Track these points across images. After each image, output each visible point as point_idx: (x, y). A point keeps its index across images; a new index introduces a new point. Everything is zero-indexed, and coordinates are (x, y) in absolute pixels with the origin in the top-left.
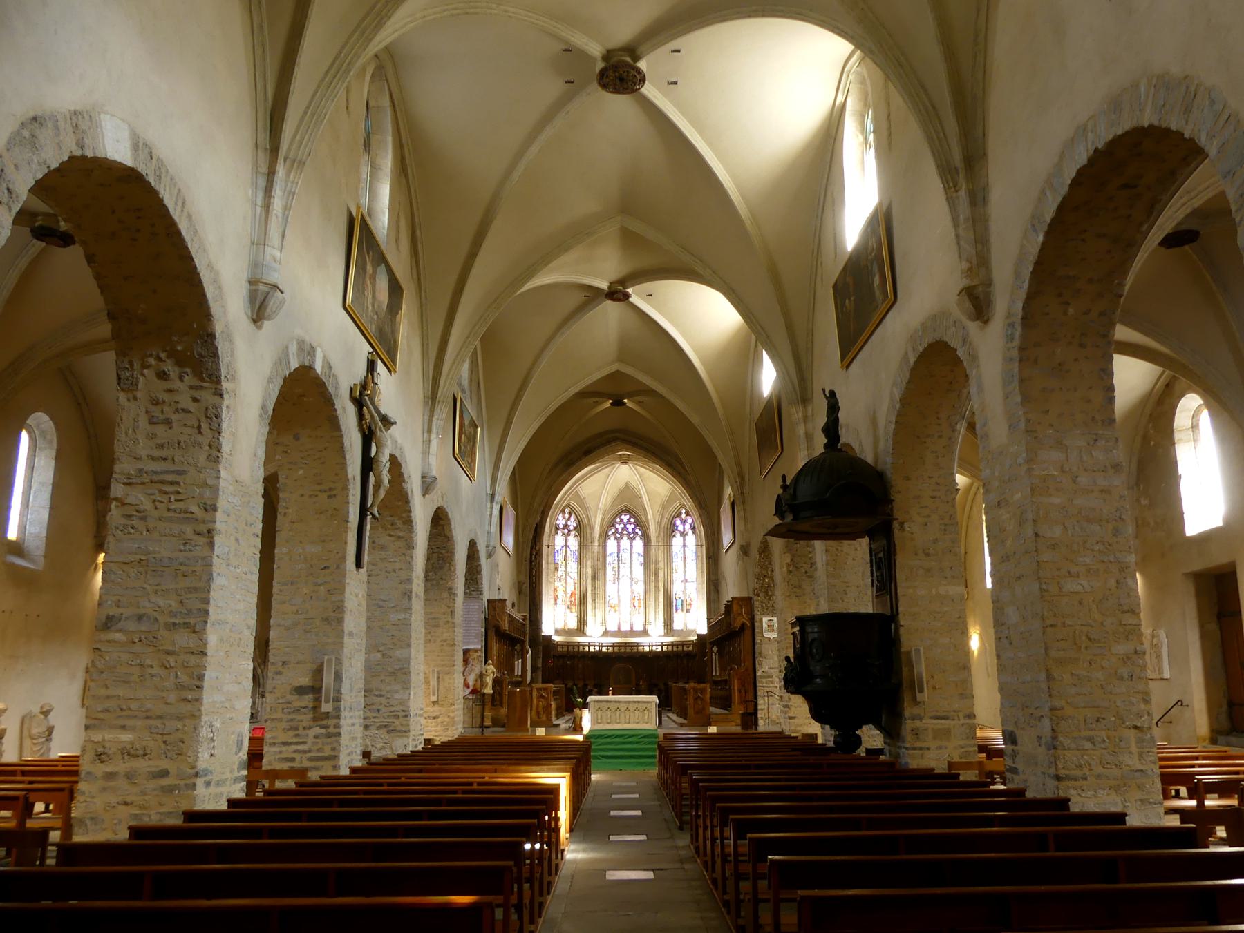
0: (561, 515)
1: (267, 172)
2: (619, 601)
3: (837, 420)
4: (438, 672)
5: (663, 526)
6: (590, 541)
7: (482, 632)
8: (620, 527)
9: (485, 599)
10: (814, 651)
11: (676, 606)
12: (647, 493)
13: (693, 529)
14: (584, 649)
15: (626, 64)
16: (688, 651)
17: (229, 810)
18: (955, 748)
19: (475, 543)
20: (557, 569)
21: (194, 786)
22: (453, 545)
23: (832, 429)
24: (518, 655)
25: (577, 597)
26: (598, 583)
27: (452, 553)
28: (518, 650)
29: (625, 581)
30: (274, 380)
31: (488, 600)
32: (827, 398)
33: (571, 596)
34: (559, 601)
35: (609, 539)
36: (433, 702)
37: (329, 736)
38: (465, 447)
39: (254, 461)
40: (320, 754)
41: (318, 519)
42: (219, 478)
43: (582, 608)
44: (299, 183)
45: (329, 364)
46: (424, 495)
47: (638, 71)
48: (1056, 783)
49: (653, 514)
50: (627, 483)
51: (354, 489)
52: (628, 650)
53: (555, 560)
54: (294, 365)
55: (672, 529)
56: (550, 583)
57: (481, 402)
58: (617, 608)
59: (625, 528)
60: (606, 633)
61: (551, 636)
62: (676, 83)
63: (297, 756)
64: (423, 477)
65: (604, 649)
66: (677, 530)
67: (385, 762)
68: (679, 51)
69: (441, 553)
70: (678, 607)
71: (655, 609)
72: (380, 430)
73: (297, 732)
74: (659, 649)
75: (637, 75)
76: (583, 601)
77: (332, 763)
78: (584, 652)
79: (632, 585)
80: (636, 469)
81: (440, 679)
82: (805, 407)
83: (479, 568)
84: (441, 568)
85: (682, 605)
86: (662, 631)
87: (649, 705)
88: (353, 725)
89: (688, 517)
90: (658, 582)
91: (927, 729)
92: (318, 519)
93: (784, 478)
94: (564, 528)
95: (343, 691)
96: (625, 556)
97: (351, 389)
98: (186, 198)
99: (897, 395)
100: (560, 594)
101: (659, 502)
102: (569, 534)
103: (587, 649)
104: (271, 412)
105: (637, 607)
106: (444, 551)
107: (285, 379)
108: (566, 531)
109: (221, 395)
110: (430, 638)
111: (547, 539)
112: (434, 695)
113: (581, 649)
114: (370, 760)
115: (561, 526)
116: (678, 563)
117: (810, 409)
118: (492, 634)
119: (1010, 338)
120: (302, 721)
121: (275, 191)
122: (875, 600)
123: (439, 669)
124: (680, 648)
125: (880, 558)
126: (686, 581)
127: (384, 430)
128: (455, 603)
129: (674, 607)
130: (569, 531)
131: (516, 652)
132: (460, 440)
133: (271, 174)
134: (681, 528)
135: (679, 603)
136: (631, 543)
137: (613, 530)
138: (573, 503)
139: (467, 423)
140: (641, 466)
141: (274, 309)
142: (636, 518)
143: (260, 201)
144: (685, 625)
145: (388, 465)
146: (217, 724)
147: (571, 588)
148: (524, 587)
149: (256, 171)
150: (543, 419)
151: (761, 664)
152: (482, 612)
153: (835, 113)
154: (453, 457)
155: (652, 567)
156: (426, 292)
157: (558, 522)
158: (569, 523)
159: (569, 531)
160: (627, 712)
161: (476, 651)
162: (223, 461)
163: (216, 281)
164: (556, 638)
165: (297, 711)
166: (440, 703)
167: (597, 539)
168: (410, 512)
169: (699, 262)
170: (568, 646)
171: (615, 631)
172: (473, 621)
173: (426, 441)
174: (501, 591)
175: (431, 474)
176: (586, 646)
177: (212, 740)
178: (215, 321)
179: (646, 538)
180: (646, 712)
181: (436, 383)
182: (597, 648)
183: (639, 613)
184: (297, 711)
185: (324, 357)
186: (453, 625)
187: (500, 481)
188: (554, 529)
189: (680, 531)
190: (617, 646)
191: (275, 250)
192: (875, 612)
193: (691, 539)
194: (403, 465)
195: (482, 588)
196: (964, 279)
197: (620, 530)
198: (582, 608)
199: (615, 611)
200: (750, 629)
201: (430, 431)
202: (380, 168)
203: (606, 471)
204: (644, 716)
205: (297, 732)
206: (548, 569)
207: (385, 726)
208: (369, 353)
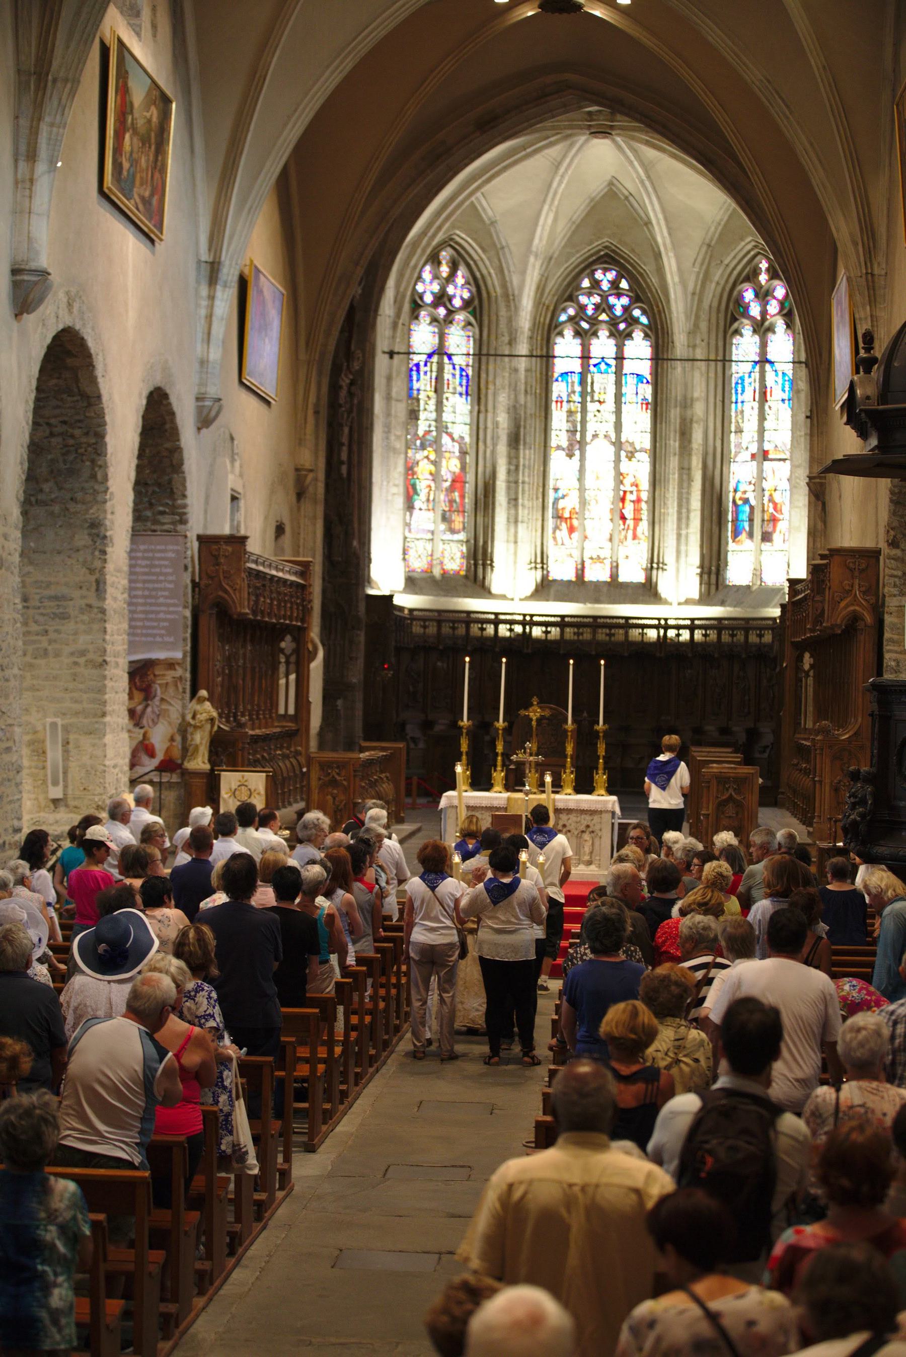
0: (428, 268)
2: (583, 502)
4: (66, 729)
6: (506, 339)
7: (185, 617)
8: (590, 302)
9: (192, 535)
11: (735, 520)
12: (664, 211)
13: (788, 316)
14: (483, 629)
16: (760, 646)
19: (165, 396)
20: (414, 415)
22: (101, 415)
24: (288, 663)
25: (469, 488)
27: (100, 436)
28: (288, 652)
31: (200, 538)
33: (451, 489)
34: (418, 503)
35: (561, 334)
36: (55, 802)
38: (134, 162)
43: (480, 519)
50: (611, 184)
52: (601, 635)
53: (411, 389)
56: (395, 451)
57: (183, 27)
58: (575, 523)
59: (604, 307)
61: (391, 597)
64: (15, 272)
66: (746, 314)
70: (741, 525)
71: (679, 528)
79: (617, 460)
81: (71, 746)
83: (176, 455)
84: (72, 472)
85: (751, 520)
86: (692, 586)
87: (596, 818)
89: (776, 282)
90: (690, 455)
96: (603, 382)
100: (423, 483)
101: (697, 237)
102: (449, 320)
105: (630, 522)
106: (77, 432)
108: (442, 311)
110: (45, 644)
111: (388, 333)
113: (475, 629)
115: (428, 298)
118: (208, 623)
123: (66, 721)
124: (740, 637)
126: (765, 455)
128: (105, 561)
130: (450, 312)
131: (283, 660)
132: (118, 150)
134: (755, 310)
135: (744, 516)
136: (620, 348)
137: (571, 312)
138: (461, 236)
139: (138, 95)
140: (647, 143)
142: (632, 280)
144: (757, 573)
147: (451, 466)
150: (348, 65)
152: (186, 568)
155: (674, 414)
157: (420, 288)
158: (450, 290)
159: (450, 312)
161: (171, 665)
164: (406, 601)
166: (72, 803)
171: (570, 582)
172: (165, 589)
173: (23, 181)
174: (242, 503)
175: (33, 265)
176: (489, 621)
180: (586, 836)
181: (48, 32)
182: (518, 629)
183: (635, 537)
186: (100, 616)
188: (407, 307)
189: (752, 318)
190: (700, 627)
195: (185, 506)
197: (590, 312)
198: (480, 519)
199: (571, 530)
203: (554, 152)
206: (388, 414)
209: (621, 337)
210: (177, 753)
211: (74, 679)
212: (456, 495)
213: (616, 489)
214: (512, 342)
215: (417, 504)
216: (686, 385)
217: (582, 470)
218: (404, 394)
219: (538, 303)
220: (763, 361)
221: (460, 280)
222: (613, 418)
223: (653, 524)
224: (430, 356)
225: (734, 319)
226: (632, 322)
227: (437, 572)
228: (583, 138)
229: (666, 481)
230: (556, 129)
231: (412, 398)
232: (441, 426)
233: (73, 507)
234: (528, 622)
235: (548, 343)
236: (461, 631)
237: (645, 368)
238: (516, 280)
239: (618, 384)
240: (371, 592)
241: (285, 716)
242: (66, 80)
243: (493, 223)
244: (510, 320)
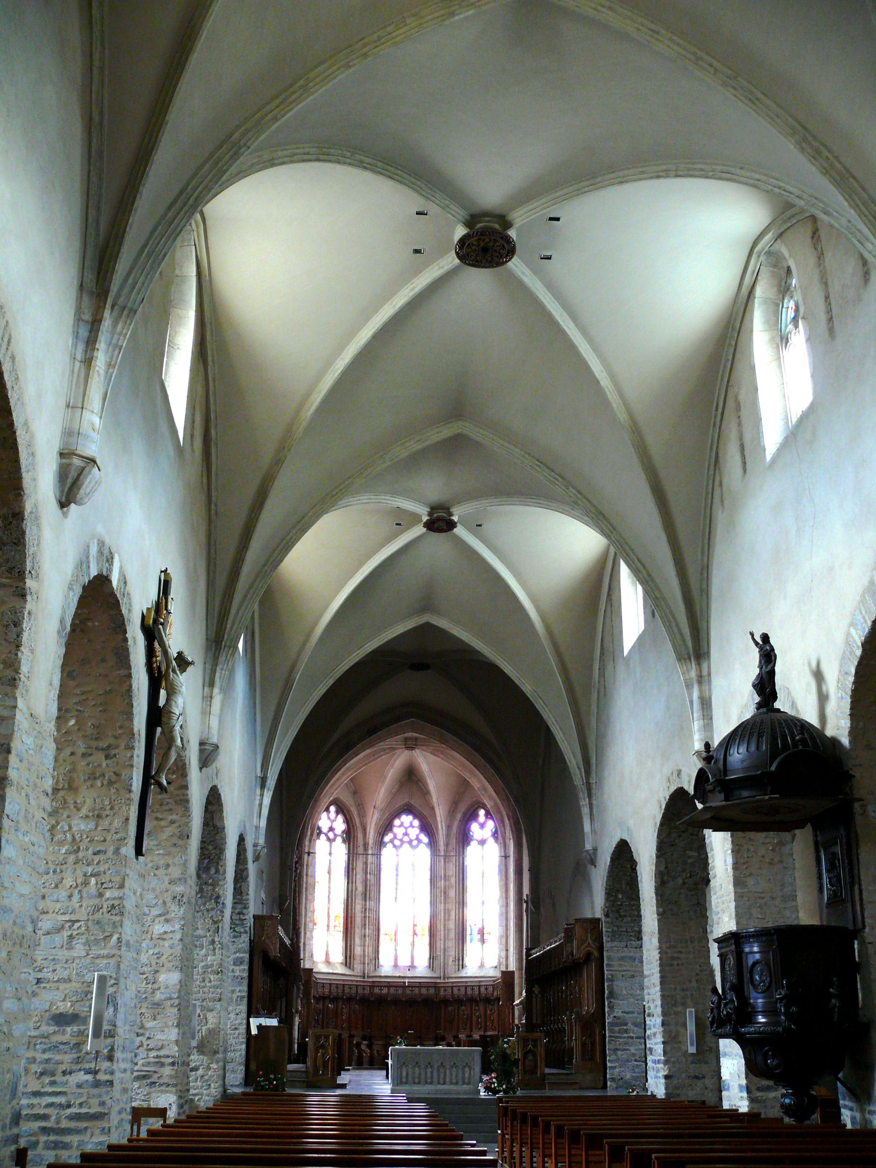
1: (90, 320)
3: (772, 673)
10: (757, 977)
15: (493, 232)
17: (82, 1164)
30: (74, 587)
32: (757, 643)
37: (97, 1084)
39: (50, 691)
41: (92, 786)
44: (128, 336)
45: (125, 578)
46: (201, 769)
47: (508, 240)
51: (139, 748)
54: (94, 572)
62: (549, 258)
67: (177, 1124)
68: (558, 219)
69: (207, 849)
72: (174, 671)
73: (53, 1079)
75: (505, 245)
83: (245, 873)
92: (92, 786)
97: (143, 616)
98: (13, 336)
99: (856, 638)
104: (68, 629)
106: (210, 847)
107: (84, 588)
109: (23, 596)
114: (165, 1121)
117: (705, 666)
118: (258, 962)
121: (100, 342)
122: (825, 910)
127: (178, 672)
130: (336, 835)
141: (88, 491)
143: (79, 355)
149: (78, 319)
151: (611, 1008)
153: (740, 301)
156: (216, 506)
158: (335, 825)
160: (442, 1070)
163: (29, 445)
165: (55, 1048)
169: (560, 479)
175: (211, 741)
178: (25, 497)
184: (55, 1048)
187: (275, 755)
191: (94, 415)
192: (825, 923)
193: (493, 850)
201: (212, 684)
202: (178, 348)
205: (53, 1079)
207: (144, 1077)
208: (162, 572)
242: (230, 647)
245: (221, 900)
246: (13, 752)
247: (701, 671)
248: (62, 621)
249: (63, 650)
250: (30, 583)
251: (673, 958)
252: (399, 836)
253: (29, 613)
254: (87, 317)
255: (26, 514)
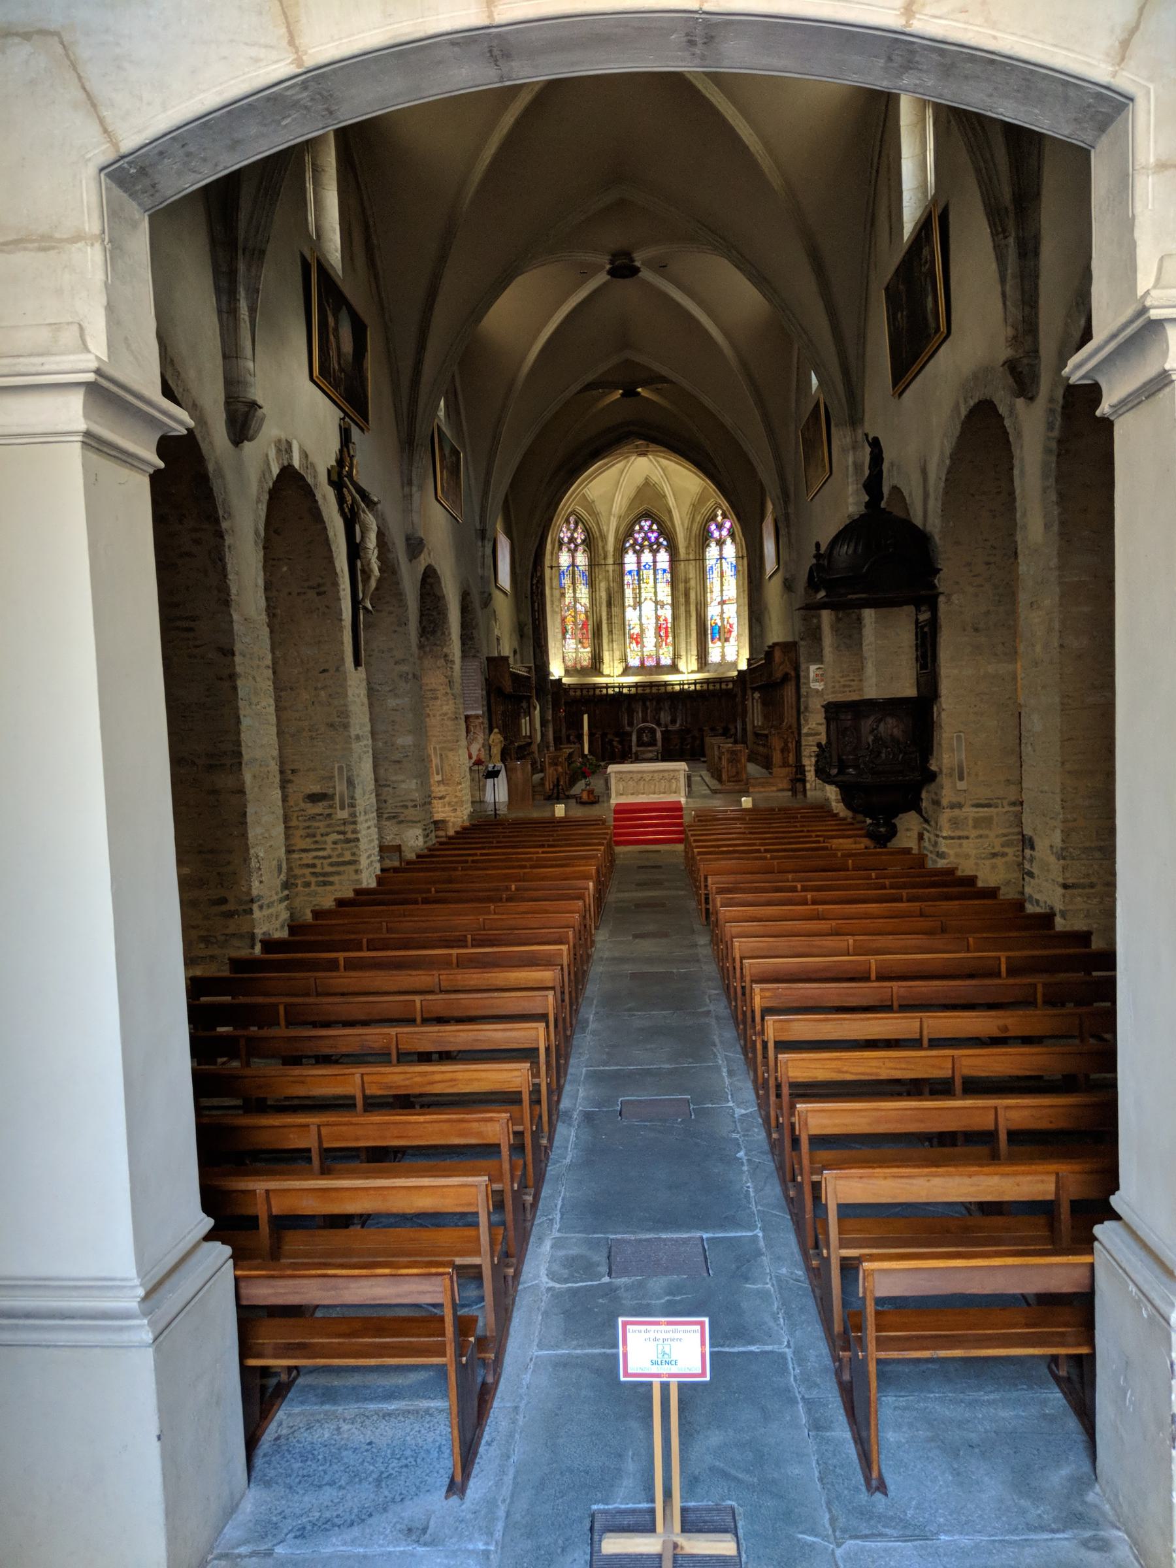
5: (694, 532)
12: (672, 489)
13: (732, 535)
16: (727, 690)
18: (997, 836)
20: (563, 595)
21: (251, 912)
23: (873, 485)
25: (590, 627)
26: (615, 610)
29: (648, 607)
33: (582, 629)
37: (348, 841)
40: (341, 860)
42: (232, 622)
46: (410, 561)
48: (1063, 891)
49: (681, 518)
50: (646, 479)
51: (344, 583)
52: (654, 690)
54: (276, 471)
55: (704, 539)
56: (557, 613)
59: (646, 538)
60: (627, 671)
63: (317, 862)
65: (625, 691)
66: (712, 537)
72: (364, 511)
74: (692, 687)
76: (597, 634)
77: (352, 867)
78: (601, 696)
79: (656, 610)
80: (658, 462)
82: (854, 430)
84: (434, 632)
85: (719, 633)
86: (694, 665)
88: (369, 828)
91: (966, 818)
93: (818, 545)
94: (569, 543)
95: (357, 796)
96: (648, 574)
102: (576, 550)
103: (604, 691)
106: (435, 613)
108: (572, 546)
112: (438, 774)
113: (597, 692)
115: (566, 540)
116: (714, 581)
119: (1050, 427)
120: (319, 828)
125: (926, 632)
129: (709, 636)
130: (576, 546)
133: (232, 274)
134: (716, 534)
137: (631, 542)
138: (579, 509)
140: (664, 458)
142: (659, 525)
145: (376, 552)
146: (261, 855)
148: (525, 629)
151: (806, 721)
154: (434, 500)
155: (681, 586)
157: (562, 535)
158: (576, 535)
161: (477, 717)
162: (233, 604)
167: (612, 553)
168: (398, 584)
170: (582, 690)
176: (604, 687)
177: (260, 869)
179: (672, 549)
185: (300, 446)
190: (641, 686)
193: (730, 550)
194: (387, 534)
196: (1009, 349)
200: (796, 677)
201: (410, 483)
203: (620, 465)
204: (670, 786)
206: (552, 595)
207: (394, 817)
209: (655, 552)
210: (482, 757)
211: (442, 725)
212: (585, 631)
213: (657, 623)
214: (605, 558)
215: (568, 636)
216: (686, 573)
217: (640, 616)
218: (558, 587)
219: (616, 538)
220: (721, 558)
221: (580, 531)
222: (653, 590)
223: (674, 638)
224: (568, 567)
225: (707, 539)
226: (660, 545)
227: (578, 667)
228: (633, 458)
229: (679, 618)
230: (621, 454)
231: (562, 587)
232: (575, 600)
233: (435, 648)
234: (621, 687)
235: (622, 557)
236: (591, 692)
237: (666, 566)
238: (605, 528)
239: (655, 574)
240: (552, 678)
241: (526, 736)
243: (593, 502)
244: (603, 548)
245: (450, 658)
246: (237, 653)
247: (856, 436)
248: (257, 532)
249: (262, 554)
250: (225, 525)
251: (844, 686)
252: (640, 540)
253: (229, 547)
254: (224, 269)
255: (211, 476)
